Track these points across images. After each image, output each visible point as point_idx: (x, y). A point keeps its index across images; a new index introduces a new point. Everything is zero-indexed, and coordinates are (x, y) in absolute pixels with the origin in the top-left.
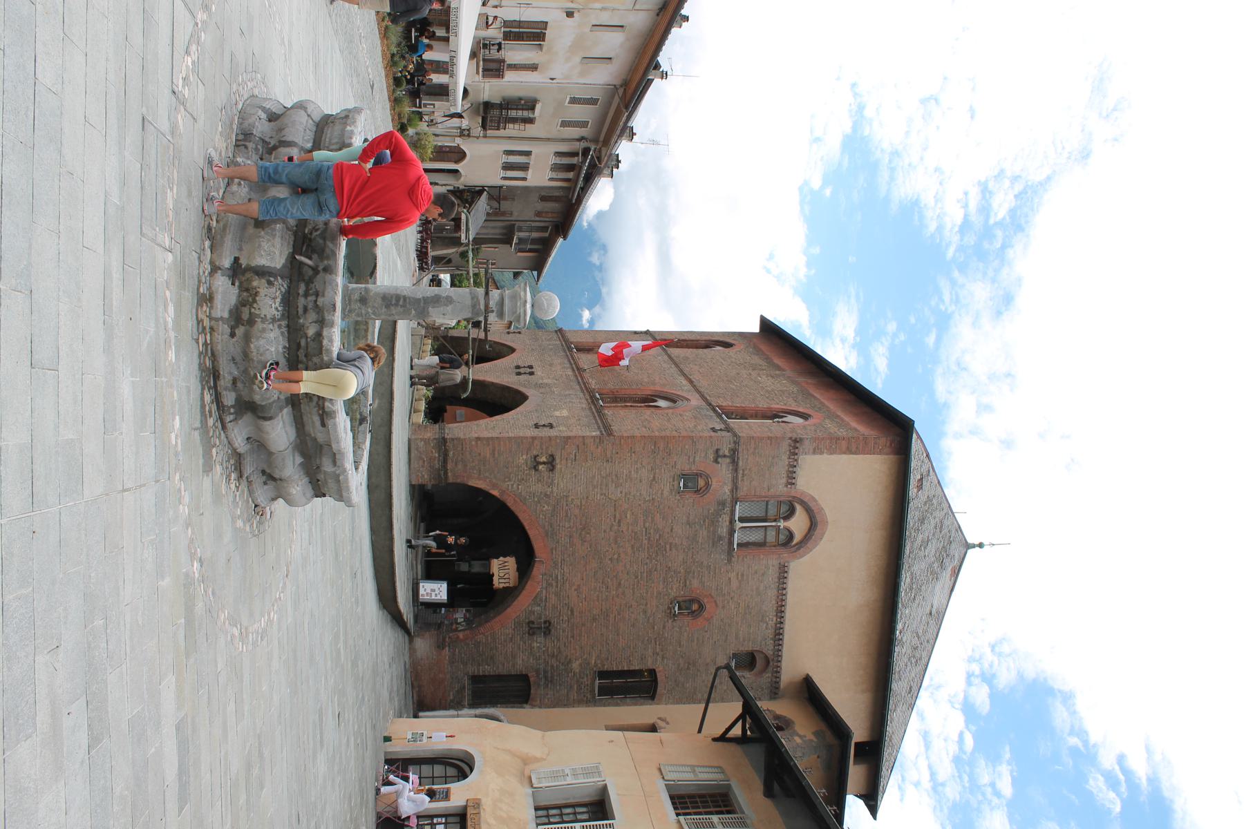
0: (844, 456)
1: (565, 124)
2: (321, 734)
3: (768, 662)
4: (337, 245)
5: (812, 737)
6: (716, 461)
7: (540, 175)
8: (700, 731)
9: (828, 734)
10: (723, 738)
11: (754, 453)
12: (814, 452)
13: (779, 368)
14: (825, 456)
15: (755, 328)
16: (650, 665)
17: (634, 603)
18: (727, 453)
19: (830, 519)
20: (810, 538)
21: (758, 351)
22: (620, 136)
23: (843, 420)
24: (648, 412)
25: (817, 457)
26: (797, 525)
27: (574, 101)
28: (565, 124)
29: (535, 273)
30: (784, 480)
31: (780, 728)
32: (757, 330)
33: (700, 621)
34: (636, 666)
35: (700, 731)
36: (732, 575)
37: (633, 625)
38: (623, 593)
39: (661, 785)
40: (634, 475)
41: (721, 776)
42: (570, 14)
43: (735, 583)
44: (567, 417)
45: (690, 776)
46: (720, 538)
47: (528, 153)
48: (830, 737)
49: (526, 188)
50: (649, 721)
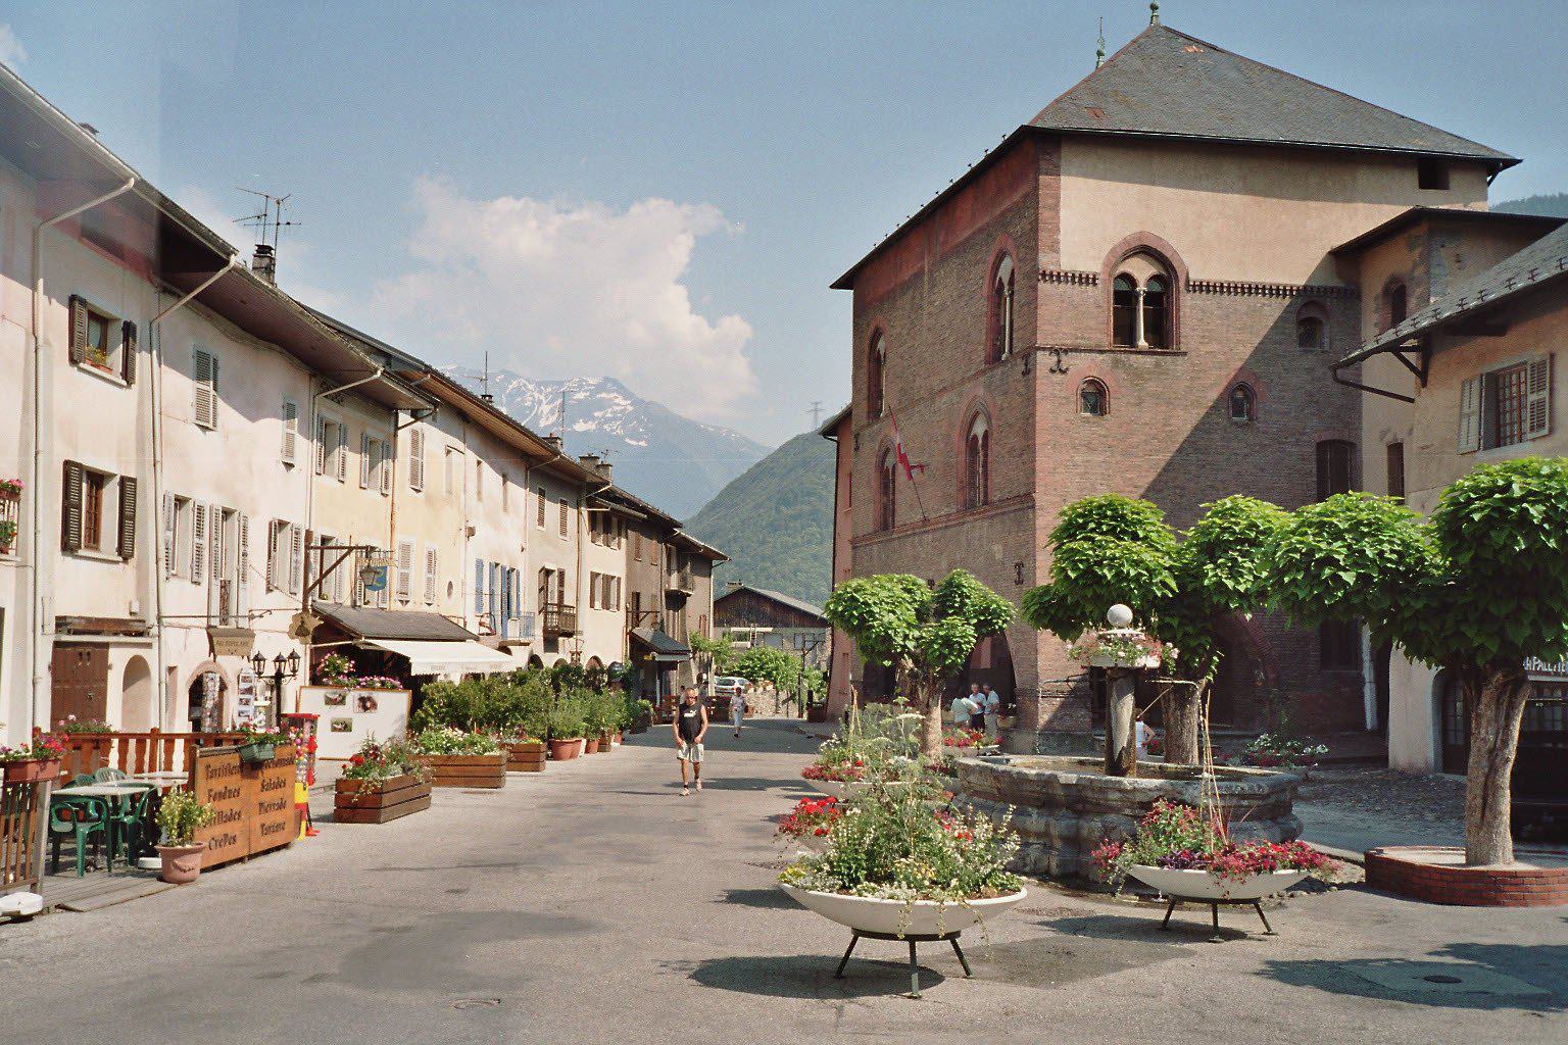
0: (1062, 213)
1: (564, 532)
2: (642, 793)
3: (1313, 303)
4: (1450, 844)
5: (1417, 252)
6: (1063, 372)
7: (611, 558)
8: (1411, 400)
9: (1415, 232)
10: (1423, 375)
11: (1057, 326)
12: (1057, 252)
13: (919, 275)
14: (1061, 237)
15: (848, 295)
16: (1311, 450)
17: (1236, 469)
18: (1055, 359)
19: (1138, 230)
20: (1160, 254)
21: (890, 296)
22: (556, 453)
23: (1009, 210)
24: (994, 448)
25: (1062, 247)
26: (1142, 271)
27: (541, 521)
28: (564, 532)
29: (714, 562)
30: (1090, 287)
31: (1495, 388)
32: (851, 292)
33: (1259, 389)
34: (1312, 467)
35: (1411, 400)
36: (1204, 349)
37: (1262, 470)
38: (1223, 482)
39: (1481, 455)
40: (1081, 470)
41: (1476, 385)
42: (471, 532)
43: (1214, 347)
44: (1005, 545)
45: (1474, 420)
46: (1158, 365)
47: (594, 576)
48: (1421, 230)
49: (628, 576)
50: (1383, 456)
